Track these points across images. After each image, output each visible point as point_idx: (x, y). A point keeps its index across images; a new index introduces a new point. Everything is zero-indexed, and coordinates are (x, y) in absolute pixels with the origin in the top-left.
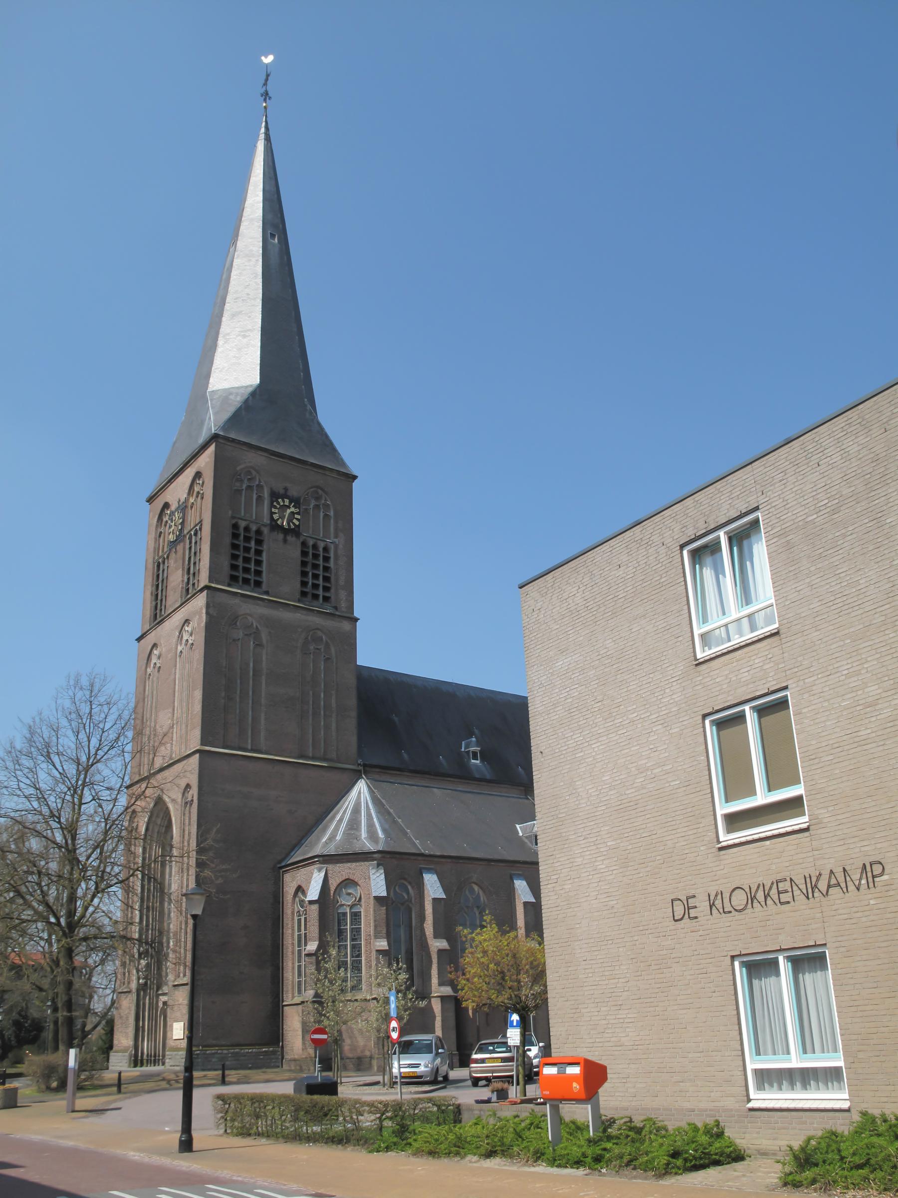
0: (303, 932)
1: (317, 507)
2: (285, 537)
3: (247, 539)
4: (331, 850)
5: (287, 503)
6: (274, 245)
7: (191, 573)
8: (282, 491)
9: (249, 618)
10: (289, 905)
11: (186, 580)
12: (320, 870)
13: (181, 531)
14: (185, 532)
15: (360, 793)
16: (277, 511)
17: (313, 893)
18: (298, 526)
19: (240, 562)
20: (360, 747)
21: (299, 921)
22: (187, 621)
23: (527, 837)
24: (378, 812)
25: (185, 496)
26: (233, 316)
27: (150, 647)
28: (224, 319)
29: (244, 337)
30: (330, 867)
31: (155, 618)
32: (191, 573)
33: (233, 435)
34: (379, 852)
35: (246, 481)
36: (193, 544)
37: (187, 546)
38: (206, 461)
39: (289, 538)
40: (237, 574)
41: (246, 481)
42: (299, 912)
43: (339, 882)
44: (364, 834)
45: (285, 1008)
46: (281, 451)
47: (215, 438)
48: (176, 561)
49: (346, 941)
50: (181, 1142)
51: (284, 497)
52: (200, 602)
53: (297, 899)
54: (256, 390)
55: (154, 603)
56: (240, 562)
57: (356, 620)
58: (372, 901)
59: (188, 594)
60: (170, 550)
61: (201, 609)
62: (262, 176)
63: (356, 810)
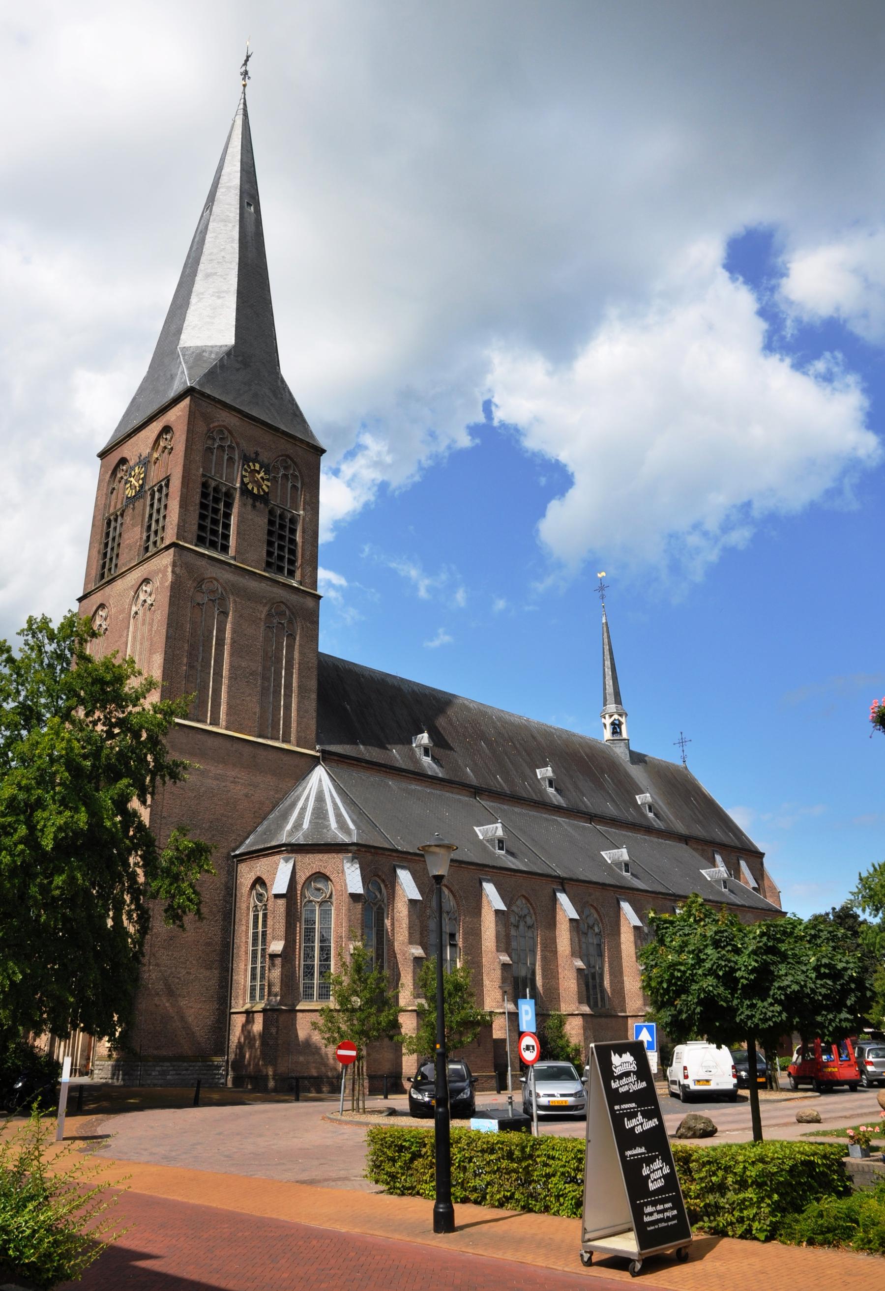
0: (260, 929)
1: (285, 476)
2: (254, 502)
3: (216, 500)
4: (299, 838)
5: (257, 468)
6: (250, 213)
7: (152, 530)
8: (253, 456)
9: (215, 582)
10: (244, 899)
11: (145, 538)
12: (287, 860)
13: (141, 486)
14: (147, 488)
15: (320, 780)
16: (247, 474)
17: (280, 886)
18: (267, 494)
19: (208, 523)
20: (317, 734)
21: (256, 917)
22: (146, 581)
23: (488, 841)
24: (344, 802)
25: (148, 450)
26: (208, 276)
27: (94, 608)
28: (198, 278)
29: (219, 297)
30: (299, 857)
31: (102, 576)
32: (152, 530)
33: (208, 391)
34: (353, 844)
35: (218, 440)
36: (156, 501)
37: (148, 503)
38: (178, 415)
39: (258, 504)
40: (204, 535)
41: (218, 440)
42: (256, 906)
43: (308, 875)
44: (333, 824)
45: (299, 1015)
46: (254, 413)
47: (189, 392)
48: (133, 518)
49: (313, 942)
50: (436, 1213)
51: (255, 461)
52: (166, 560)
53: (254, 892)
54: (230, 350)
55: (101, 562)
56: (208, 523)
57: (320, 597)
58: (346, 899)
59: (148, 552)
60: (127, 506)
61: (166, 567)
62: (240, 148)
63: (320, 798)
